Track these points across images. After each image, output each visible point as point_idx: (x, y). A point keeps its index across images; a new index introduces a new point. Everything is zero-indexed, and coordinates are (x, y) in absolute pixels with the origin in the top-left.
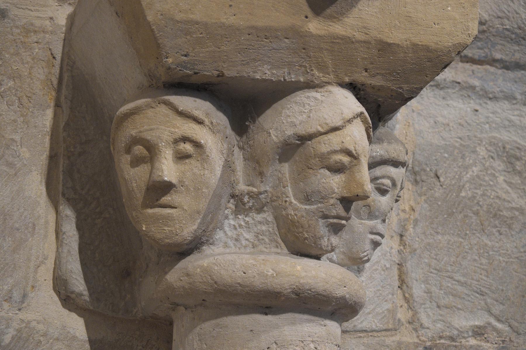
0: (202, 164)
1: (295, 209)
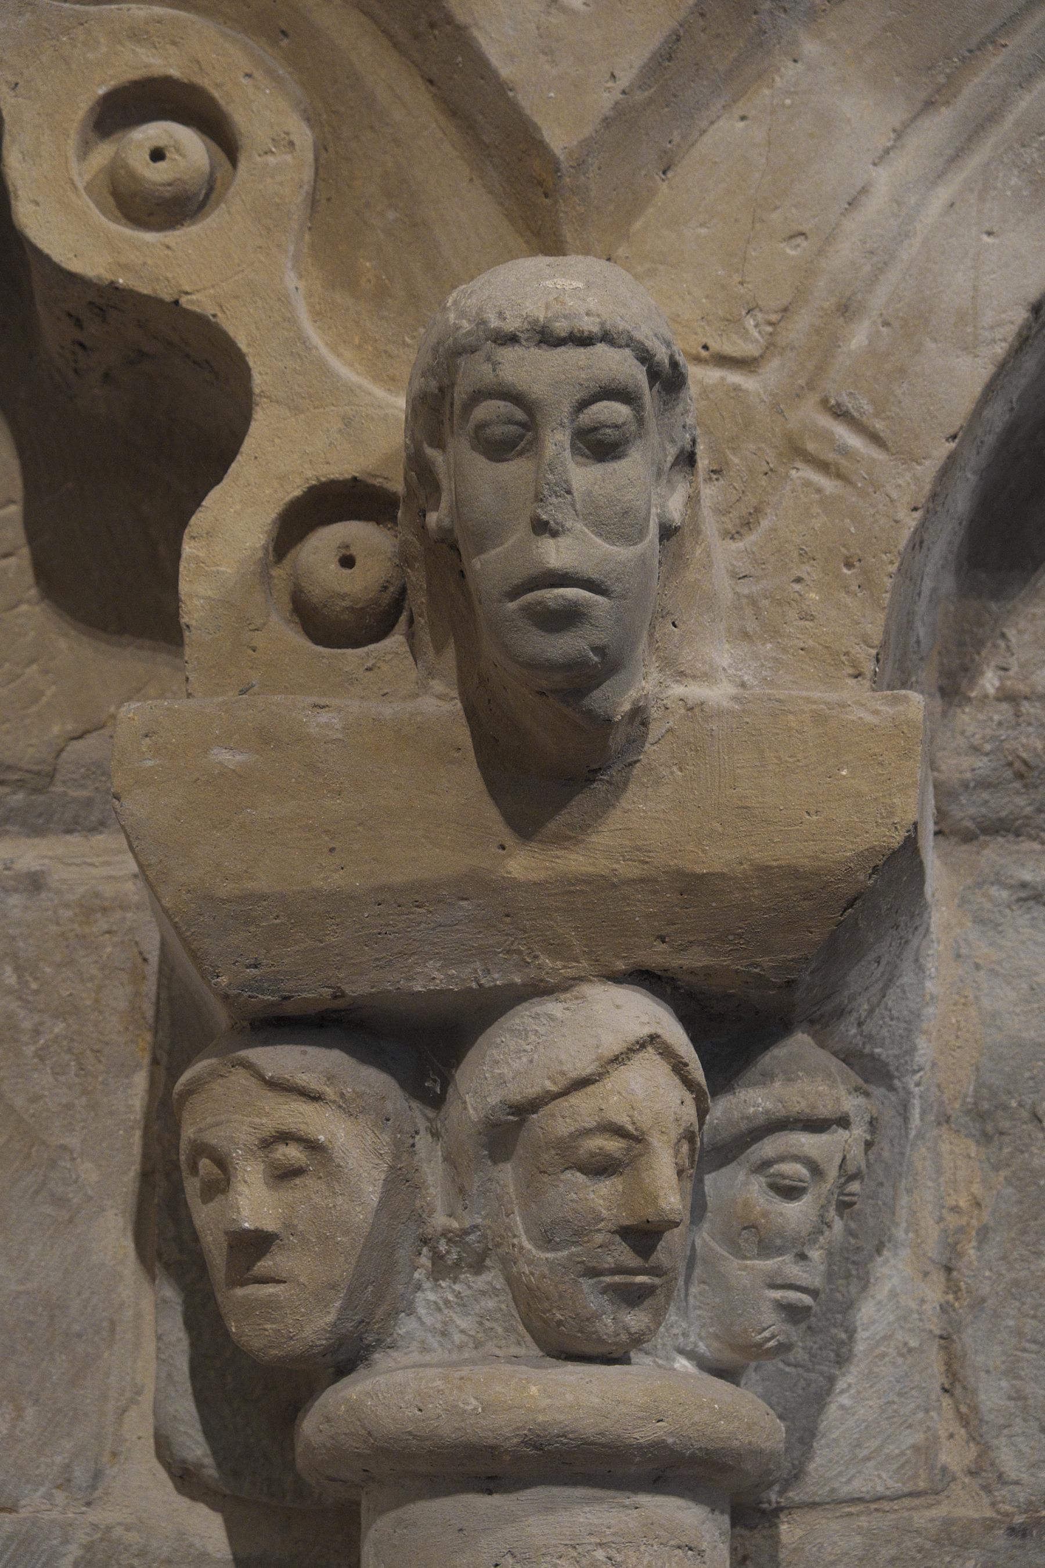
0: (328, 1185)
1: (530, 1262)
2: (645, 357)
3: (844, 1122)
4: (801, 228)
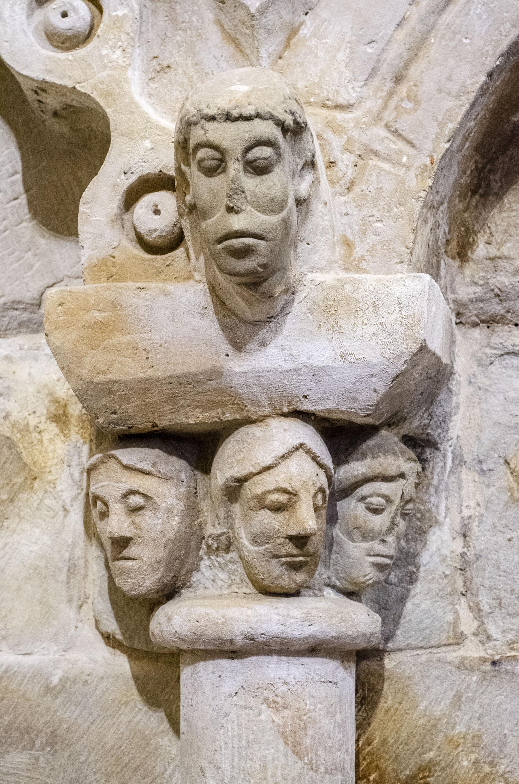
0: (154, 514)
1: (248, 551)
2: (280, 124)
3: (402, 476)
4: (374, 39)
